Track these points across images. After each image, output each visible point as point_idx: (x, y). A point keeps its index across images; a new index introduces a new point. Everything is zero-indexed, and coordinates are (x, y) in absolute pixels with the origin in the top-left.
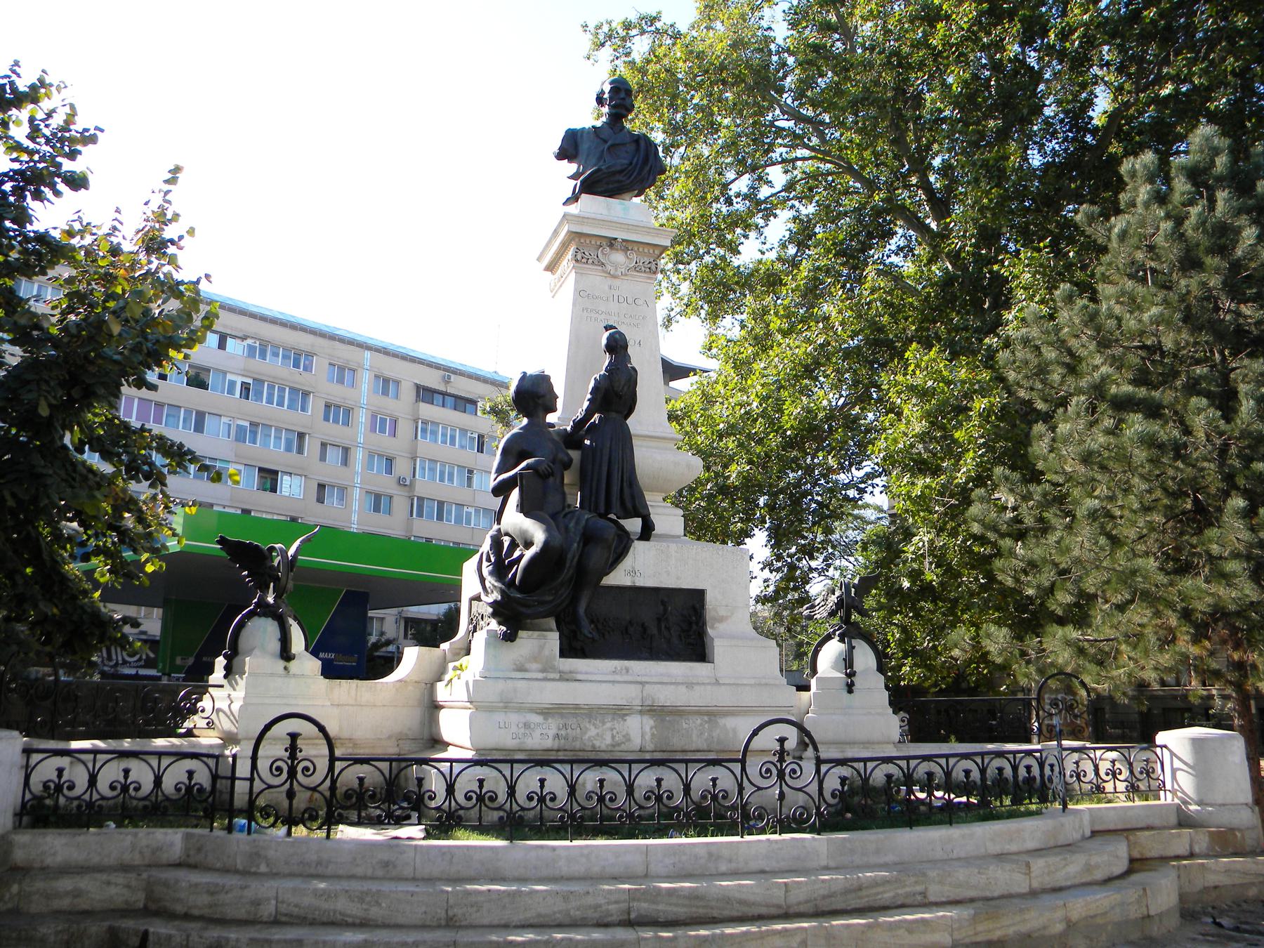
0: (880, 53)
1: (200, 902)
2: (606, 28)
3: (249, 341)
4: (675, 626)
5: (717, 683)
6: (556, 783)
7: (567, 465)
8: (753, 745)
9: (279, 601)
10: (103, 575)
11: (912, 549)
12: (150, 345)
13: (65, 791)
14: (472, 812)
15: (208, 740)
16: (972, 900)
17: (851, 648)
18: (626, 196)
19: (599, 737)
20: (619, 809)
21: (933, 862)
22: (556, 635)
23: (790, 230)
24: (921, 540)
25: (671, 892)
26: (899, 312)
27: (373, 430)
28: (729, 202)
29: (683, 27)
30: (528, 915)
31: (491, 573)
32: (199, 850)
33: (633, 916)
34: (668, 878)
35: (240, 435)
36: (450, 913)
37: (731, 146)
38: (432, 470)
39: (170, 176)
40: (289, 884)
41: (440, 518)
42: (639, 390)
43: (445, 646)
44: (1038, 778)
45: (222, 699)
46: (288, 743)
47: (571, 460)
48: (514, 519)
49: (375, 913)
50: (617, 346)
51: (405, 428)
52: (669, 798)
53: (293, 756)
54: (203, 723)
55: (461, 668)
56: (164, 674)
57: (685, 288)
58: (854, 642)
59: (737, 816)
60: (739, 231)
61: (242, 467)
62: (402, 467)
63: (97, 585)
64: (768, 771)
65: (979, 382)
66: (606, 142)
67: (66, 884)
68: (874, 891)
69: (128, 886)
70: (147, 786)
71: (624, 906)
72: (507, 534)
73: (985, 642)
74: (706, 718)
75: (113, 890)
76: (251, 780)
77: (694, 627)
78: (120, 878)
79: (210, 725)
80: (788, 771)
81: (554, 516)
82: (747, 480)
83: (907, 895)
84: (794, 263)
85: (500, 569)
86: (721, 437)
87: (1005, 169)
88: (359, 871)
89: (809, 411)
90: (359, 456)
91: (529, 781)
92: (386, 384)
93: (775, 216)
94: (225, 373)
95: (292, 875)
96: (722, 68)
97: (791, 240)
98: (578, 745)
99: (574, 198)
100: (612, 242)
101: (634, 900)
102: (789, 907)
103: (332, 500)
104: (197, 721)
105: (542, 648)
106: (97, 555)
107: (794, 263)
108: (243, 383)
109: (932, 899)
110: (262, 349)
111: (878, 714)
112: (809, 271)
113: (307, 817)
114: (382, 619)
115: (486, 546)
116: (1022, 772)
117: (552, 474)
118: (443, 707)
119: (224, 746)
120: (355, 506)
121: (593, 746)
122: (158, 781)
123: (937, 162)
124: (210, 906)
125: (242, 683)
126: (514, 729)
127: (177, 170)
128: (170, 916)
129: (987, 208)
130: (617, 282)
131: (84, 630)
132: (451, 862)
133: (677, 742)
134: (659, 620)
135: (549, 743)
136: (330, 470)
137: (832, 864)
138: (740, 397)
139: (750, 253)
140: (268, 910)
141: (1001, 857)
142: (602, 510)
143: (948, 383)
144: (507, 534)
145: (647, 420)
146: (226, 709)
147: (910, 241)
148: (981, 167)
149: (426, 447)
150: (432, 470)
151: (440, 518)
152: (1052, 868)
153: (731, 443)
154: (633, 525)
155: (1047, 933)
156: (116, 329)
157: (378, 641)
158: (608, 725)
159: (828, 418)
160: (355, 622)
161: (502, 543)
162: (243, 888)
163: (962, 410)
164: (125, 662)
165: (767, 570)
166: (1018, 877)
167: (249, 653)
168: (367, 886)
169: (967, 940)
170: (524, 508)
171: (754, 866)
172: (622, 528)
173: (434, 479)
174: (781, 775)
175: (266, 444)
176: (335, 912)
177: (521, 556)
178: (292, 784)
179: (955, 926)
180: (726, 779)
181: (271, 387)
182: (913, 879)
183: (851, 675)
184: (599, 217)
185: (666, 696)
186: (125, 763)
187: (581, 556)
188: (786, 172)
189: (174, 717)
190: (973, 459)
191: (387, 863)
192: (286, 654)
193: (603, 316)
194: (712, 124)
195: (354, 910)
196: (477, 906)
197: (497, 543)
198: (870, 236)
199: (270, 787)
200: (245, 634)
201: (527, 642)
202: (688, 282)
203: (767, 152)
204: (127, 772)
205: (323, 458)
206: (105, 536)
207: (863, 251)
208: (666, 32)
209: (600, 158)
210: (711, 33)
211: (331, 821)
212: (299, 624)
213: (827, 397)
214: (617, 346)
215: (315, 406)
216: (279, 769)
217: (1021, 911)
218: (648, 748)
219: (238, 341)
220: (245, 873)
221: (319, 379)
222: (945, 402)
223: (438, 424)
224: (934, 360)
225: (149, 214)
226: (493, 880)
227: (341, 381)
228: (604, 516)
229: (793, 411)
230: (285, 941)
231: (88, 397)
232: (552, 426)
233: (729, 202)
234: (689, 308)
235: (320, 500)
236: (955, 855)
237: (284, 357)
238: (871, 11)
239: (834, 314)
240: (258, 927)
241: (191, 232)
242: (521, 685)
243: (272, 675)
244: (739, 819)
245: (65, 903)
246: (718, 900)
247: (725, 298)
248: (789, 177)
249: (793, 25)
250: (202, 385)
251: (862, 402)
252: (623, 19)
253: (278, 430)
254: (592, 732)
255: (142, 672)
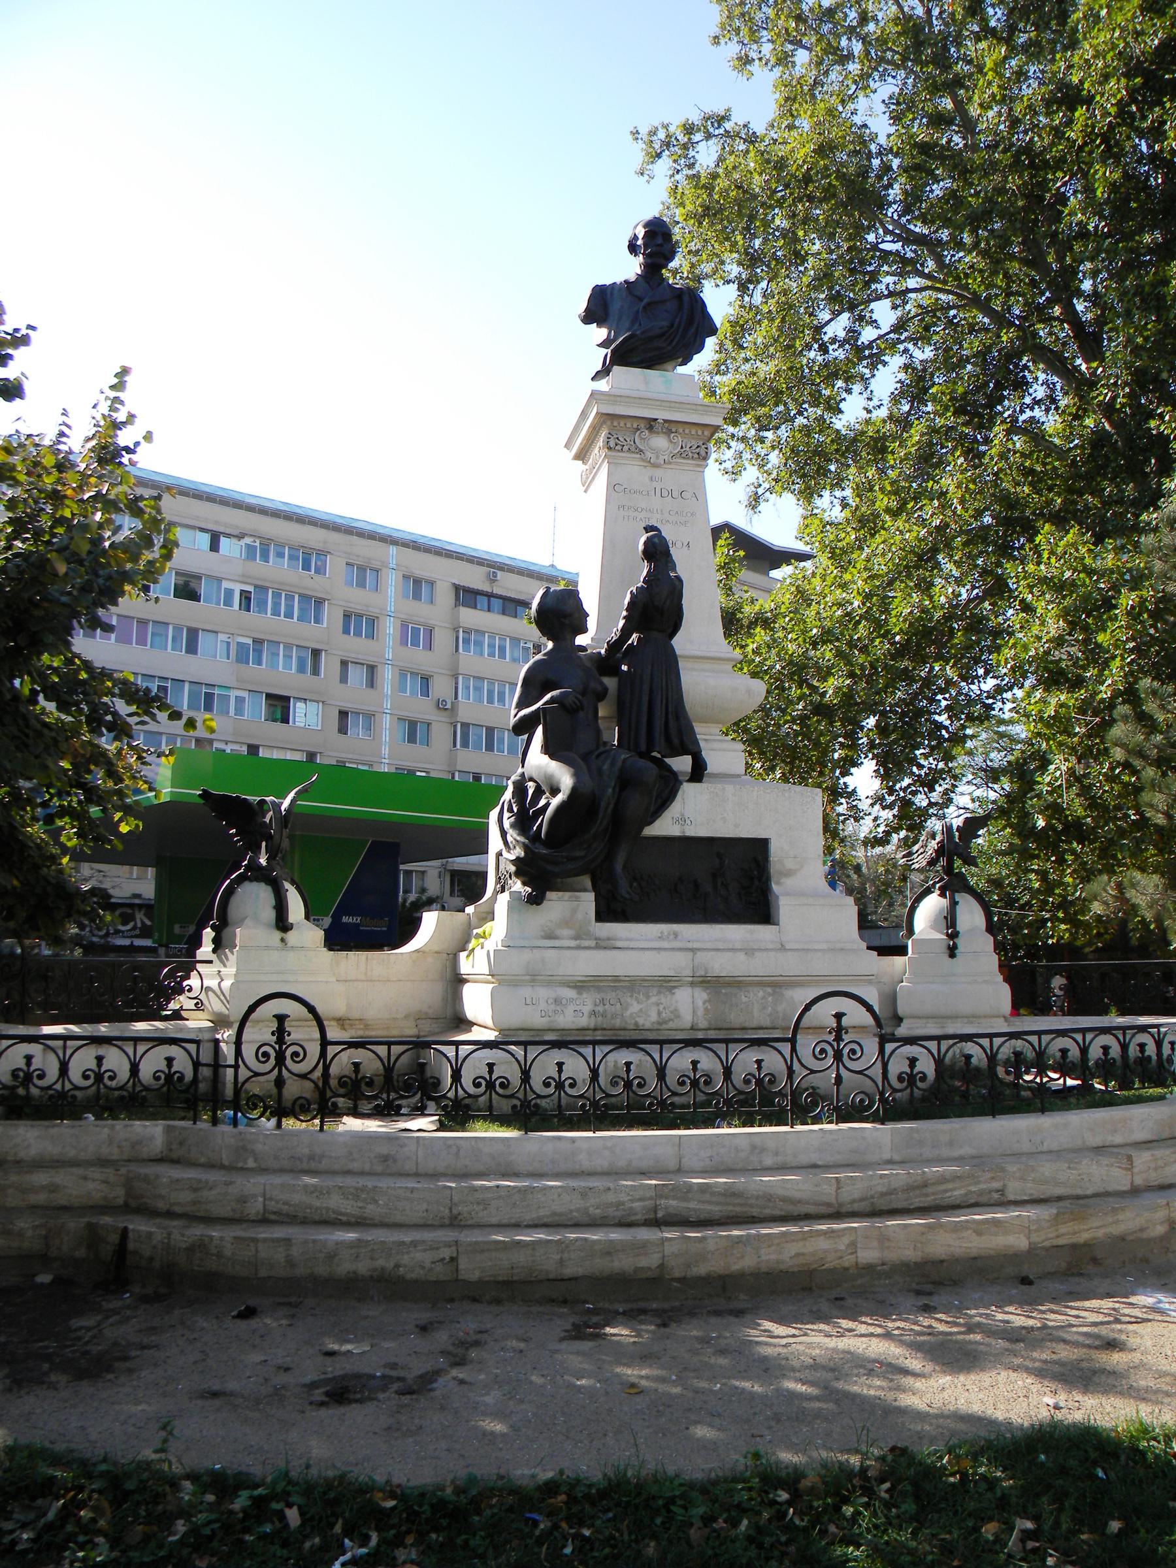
0: (1005, 151)
1: (183, 1197)
2: (662, 135)
3: (248, 540)
4: (736, 883)
5: (782, 948)
6: (576, 1067)
7: (601, 695)
8: (805, 1022)
9: (274, 863)
10: (70, 839)
11: (1048, 779)
12: (101, 581)
13: (35, 1081)
14: (482, 1099)
15: (197, 1023)
16: (1060, 1199)
17: (954, 903)
18: (669, 365)
19: (642, 1012)
20: (648, 1095)
21: (1017, 1155)
22: (591, 896)
23: (900, 382)
24: (1058, 769)
25: (703, 1188)
26: (1040, 480)
27: (404, 642)
28: (824, 349)
29: (759, 127)
30: (542, 1213)
31: (513, 826)
32: (181, 1144)
33: (660, 1214)
34: (704, 1173)
35: (242, 655)
36: (455, 1211)
37: (824, 277)
38: (478, 689)
39: (116, 381)
40: (277, 1180)
41: (490, 747)
42: (685, 602)
43: (470, 910)
44: (1154, 1057)
45: (211, 977)
46: (274, 1025)
47: (606, 690)
48: (538, 760)
49: (371, 1210)
50: (657, 551)
51: (443, 639)
52: (707, 1083)
53: (280, 1041)
54: (190, 1004)
55: (484, 936)
56: (161, 945)
57: (775, 458)
58: (958, 897)
59: (787, 1103)
60: (840, 383)
61: (245, 694)
62: (441, 688)
63: (65, 850)
64: (823, 1051)
65: (1130, 570)
66: (640, 299)
67: (41, 1178)
68: (943, 1187)
69: (106, 1182)
70: (124, 1074)
71: (649, 1203)
72: (531, 779)
73: (1130, 894)
74: (769, 990)
75: (91, 1186)
76: (236, 1067)
77: (756, 883)
78: (96, 1173)
79: (199, 1006)
80: (846, 1051)
81: (585, 757)
82: (848, 697)
83: (981, 1193)
84: (904, 423)
85: (524, 821)
86: (814, 645)
87: (1164, 296)
88: (356, 1166)
89: (924, 610)
90: (387, 676)
91: (545, 1066)
92: (417, 586)
93: (885, 364)
94: (219, 580)
95: (282, 1171)
96: (807, 179)
97: (902, 394)
98: (618, 1023)
99: (604, 372)
100: (651, 424)
101: (661, 1197)
102: (841, 1205)
103: (357, 730)
104: (183, 1002)
105: (574, 911)
106: (61, 817)
107: (904, 423)
108: (242, 592)
109: (1012, 1197)
110: (264, 548)
111: (986, 982)
112: (922, 435)
113: (298, 1109)
114: (423, 872)
115: (508, 795)
116: (1133, 1051)
117: (582, 708)
118: (466, 981)
119: (215, 1030)
120: (386, 737)
121: (636, 1024)
122: (134, 1069)
123: (1087, 285)
124: (194, 1203)
125: (233, 958)
126: (543, 1005)
127: (124, 371)
128: (150, 1213)
129: (1142, 347)
130: (658, 473)
131: (51, 902)
132: (457, 1154)
133: (735, 1018)
134: (714, 876)
135: (583, 1021)
136: (353, 694)
137: (897, 1157)
138: (839, 594)
139: (853, 411)
140: (255, 1208)
141: (1100, 1150)
142: (643, 747)
143: (1090, 572)
144: (531, 779)
145: (698, 635)
146: (216, 988)
147: (1053, 390)
148: (1135, 295)
149: (469, 661)
150: (478, 689)
151: (490, 747)
152: (1160, 1163)
153: (827, 653)
154: (682, 764)
155: (1144, 1236)
156: (62, 568)
157: (418, 899)
158: (654, 999)
159: (948, 618)
160: (371, 879)
161: (526, 790)
162: (227, 1184)
163: (1108, 604)
164: (117, 932)
165: (877, 807)
166: (1117, 1173)
167: (240, 923)
168: (362, 1182)
169: (1047, 1244)
170: (549, 749)
171: (804, 1159)
172: (669, 769)
173: (481, 701)
174: (838, 1056)
175: (273, 665)
176: (328, 1209)
177: (548, 805)
178: (280, 1071)
179: (1033, 1228)
180: (774, 1062)
181: (277, 595)
182: (989, 1175)
183: (953, 936)
184: (635, 394)
185: (722, 965)
186: (101, 1051)
187: (616, 804)
188: (895, 307)
189: (157, 998)
190: (1122, 668)
191: (387, 1159)
192: (282, 924)
193: (643, 515)
194: (797, 254)
195: (348, 1207)
196: (485, 1204)
197: (520, 789)
198: (999, 386)
199: (256, 1074)
200: (235, 901)
201: (557, 904)
202: (777, 452)
203: (867, 284)
204: (100, 1059)
205: (344, 679)
206: (69, 794)
207: (991, 405)
208: (738, 135)
209: (633, 322)
210: (794, 133)
211: (327, 1110)
212: (298, 888)
213: (952, 587)
214: (657, 551)
215: (332, 616)
216: (265, 1054)
217: (1114, 1210)
218: (701, 1026)
219: (234, 540)
220: (231, 1168)
221: (334, 583)
222: (1086, 598)
223: (483, 633)
224: (1073, 545)
225: (99, 417)
226: (505, 1176)
227: (362, 584)
228: (645, 755)
229: (904, 606)
230: (273, 1240)
231: (37, 646)
232: (583, 648)
233: (824, 349)
234: (780, 484)
235: (343, 730)
236: (1045, 1148)
237: (291, 557)
238: (993, 95)
239: (952, 488)
240: (245, 1225)
241: (148, 437)
242: (551, 953)
243: (267, 948)
244: (801, 1106)
245: (41, 1198)
246: (758, 1198)
247: (823, 472)
248: (899, 313)
249: (896, 118)
250: (193, 596)
251: (992, 596)
252: (683, 120)
253: (288, 647)
254: (635, 1007)
255: (139, 942)
